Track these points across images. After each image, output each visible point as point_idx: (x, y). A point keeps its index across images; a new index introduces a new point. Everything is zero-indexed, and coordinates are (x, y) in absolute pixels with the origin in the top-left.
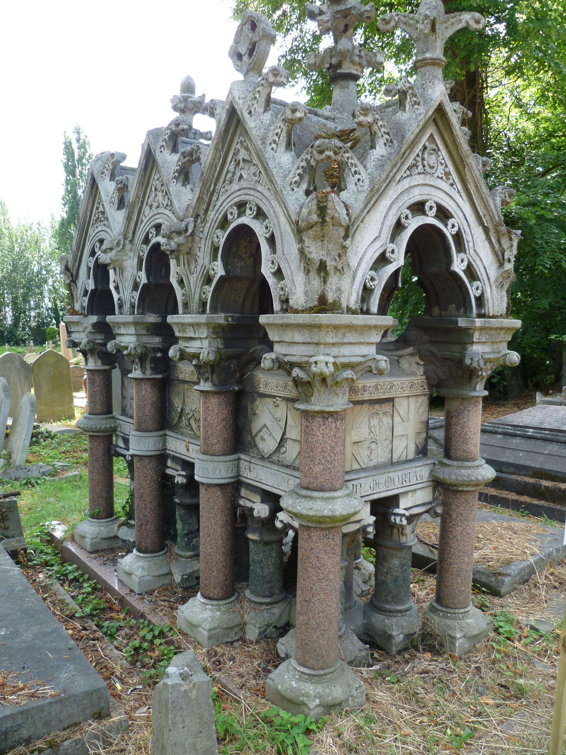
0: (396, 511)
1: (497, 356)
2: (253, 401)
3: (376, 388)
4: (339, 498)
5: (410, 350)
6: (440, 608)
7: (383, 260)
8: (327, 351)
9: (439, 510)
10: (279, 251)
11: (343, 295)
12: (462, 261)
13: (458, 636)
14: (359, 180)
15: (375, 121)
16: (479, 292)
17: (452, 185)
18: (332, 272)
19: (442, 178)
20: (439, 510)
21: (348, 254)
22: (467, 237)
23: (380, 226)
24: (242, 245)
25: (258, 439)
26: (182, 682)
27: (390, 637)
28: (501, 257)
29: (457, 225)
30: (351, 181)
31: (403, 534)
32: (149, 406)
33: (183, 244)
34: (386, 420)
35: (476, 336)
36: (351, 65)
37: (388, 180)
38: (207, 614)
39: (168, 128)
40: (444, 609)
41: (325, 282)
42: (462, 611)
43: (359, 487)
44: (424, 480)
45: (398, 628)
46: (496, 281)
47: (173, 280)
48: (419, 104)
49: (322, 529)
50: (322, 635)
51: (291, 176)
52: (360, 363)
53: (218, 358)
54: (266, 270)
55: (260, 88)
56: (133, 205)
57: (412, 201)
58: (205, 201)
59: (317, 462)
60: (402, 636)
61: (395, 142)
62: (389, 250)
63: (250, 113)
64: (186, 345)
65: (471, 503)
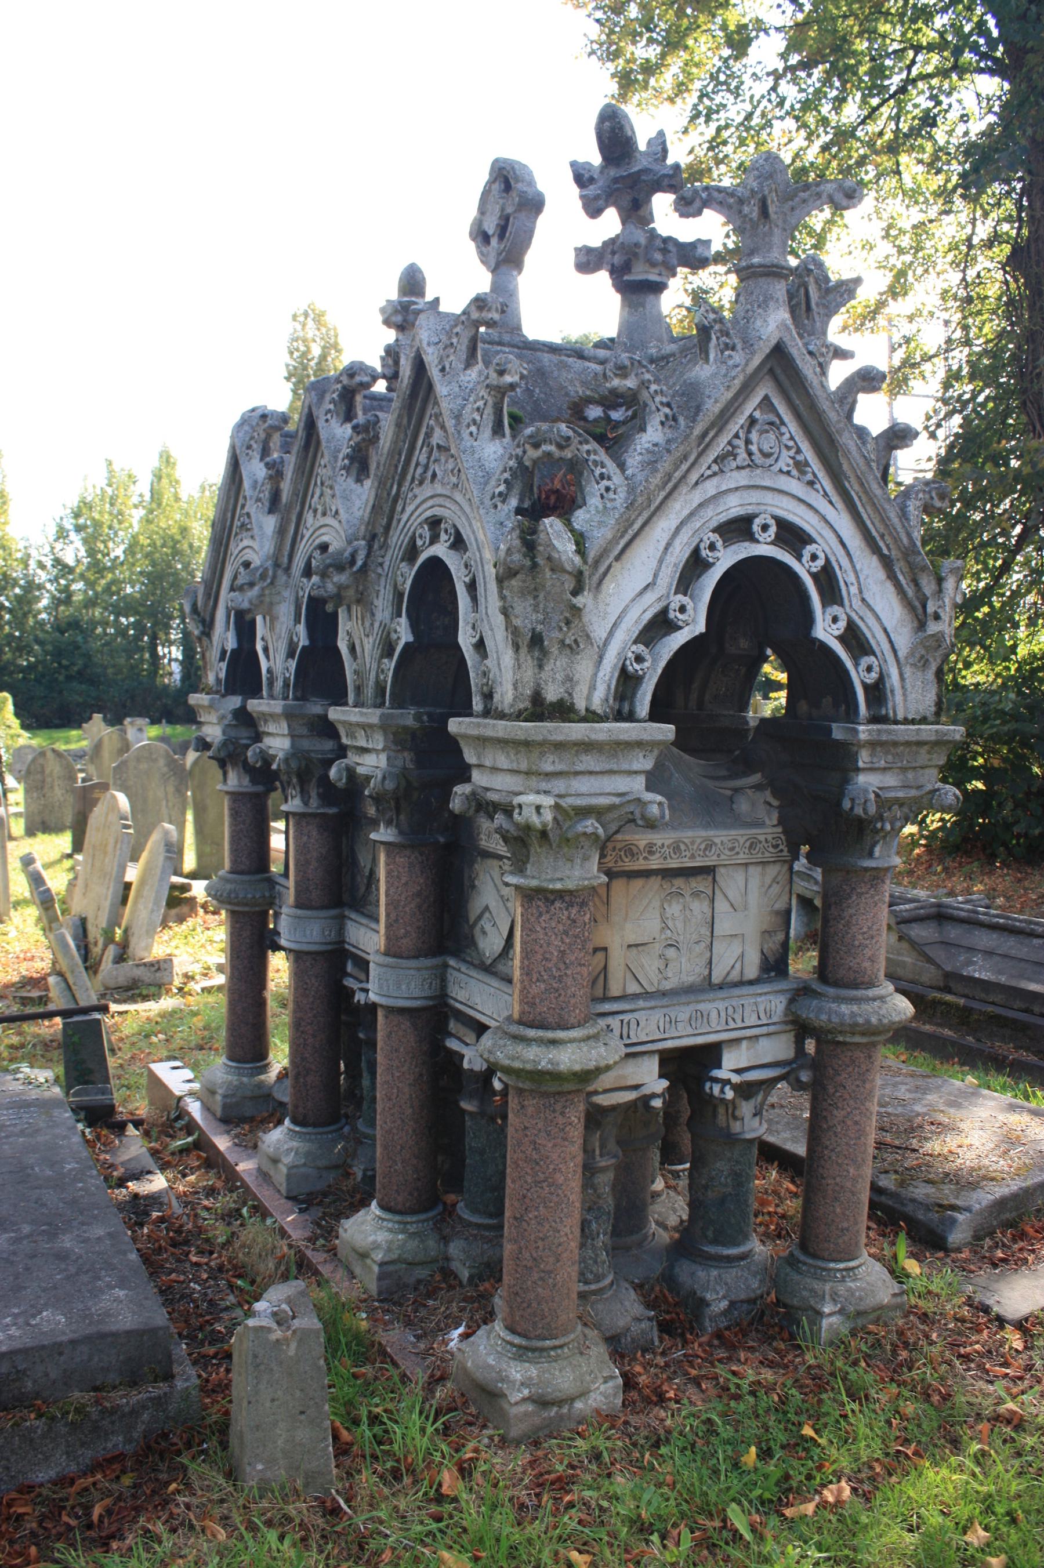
0: (716, 1073)
1: (913, 793)
2: (472, 863)
3: (676, 849)
4: (572, 1041)
5: (756, 778)
6: (802, 1258)
7: (661, 624)
8: (544, 786)
9: (805, 1076)
10: (482, 608)
11: (577, 689)
12: (835, 620)
13: (827, 1310)
14: (608, 489)
15: (644, 384)
16: (874, 675)
17: (811, 483)
18: (554, 650)
19: (788, 473)
20: (805, 1076)
21: (585, 619)
22: (844, 575)
23: (654, 564)
24: (432, 595)
25: (477, 931)
26: (274, 1326)
27: (703, 1303)
28: (920, 611)
29: (822, 555)
30: (593, 491)
31: (735, 1118)
32: (314, 864)
33: (347, 587)
34: (699, 908)
35: (864, 758)
36: (647, 267)
37: (670, 485)
38: (382, 1237)
39: (338, 381)
40: (810, 1261)
41: (541, 667)
42: (841, 1266)
43: (633, 1025)
44: (775, 1019)
45: (719, 1290)
46: (911, 653)
47: (342, 645)
48: (733, 349)
49: (545, 1095)
50: (541, 1279)
51: (493, 483)
52: (612, 808)
53: (403, 783)
54: (465, 640)
55: (458, 329)
56: (289, 507)
57: (723, 518)
58: (385, 510)
59: (535, 976)
60: (724, 1304)
61: (681, 420)
62: (675, 605)
63: (443, 370)
64: (357, 759)
65: (864, 1067)
